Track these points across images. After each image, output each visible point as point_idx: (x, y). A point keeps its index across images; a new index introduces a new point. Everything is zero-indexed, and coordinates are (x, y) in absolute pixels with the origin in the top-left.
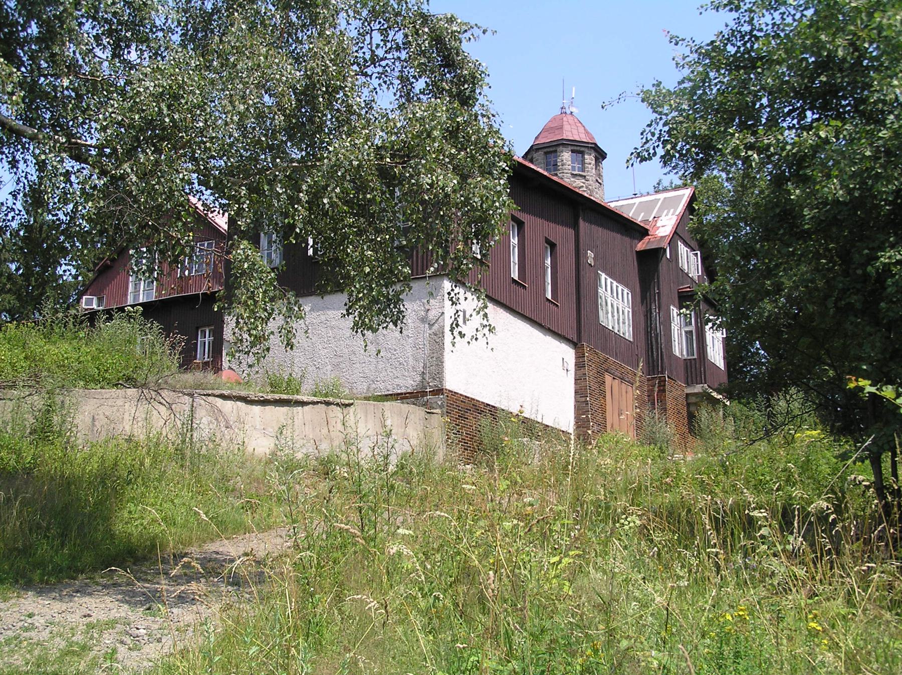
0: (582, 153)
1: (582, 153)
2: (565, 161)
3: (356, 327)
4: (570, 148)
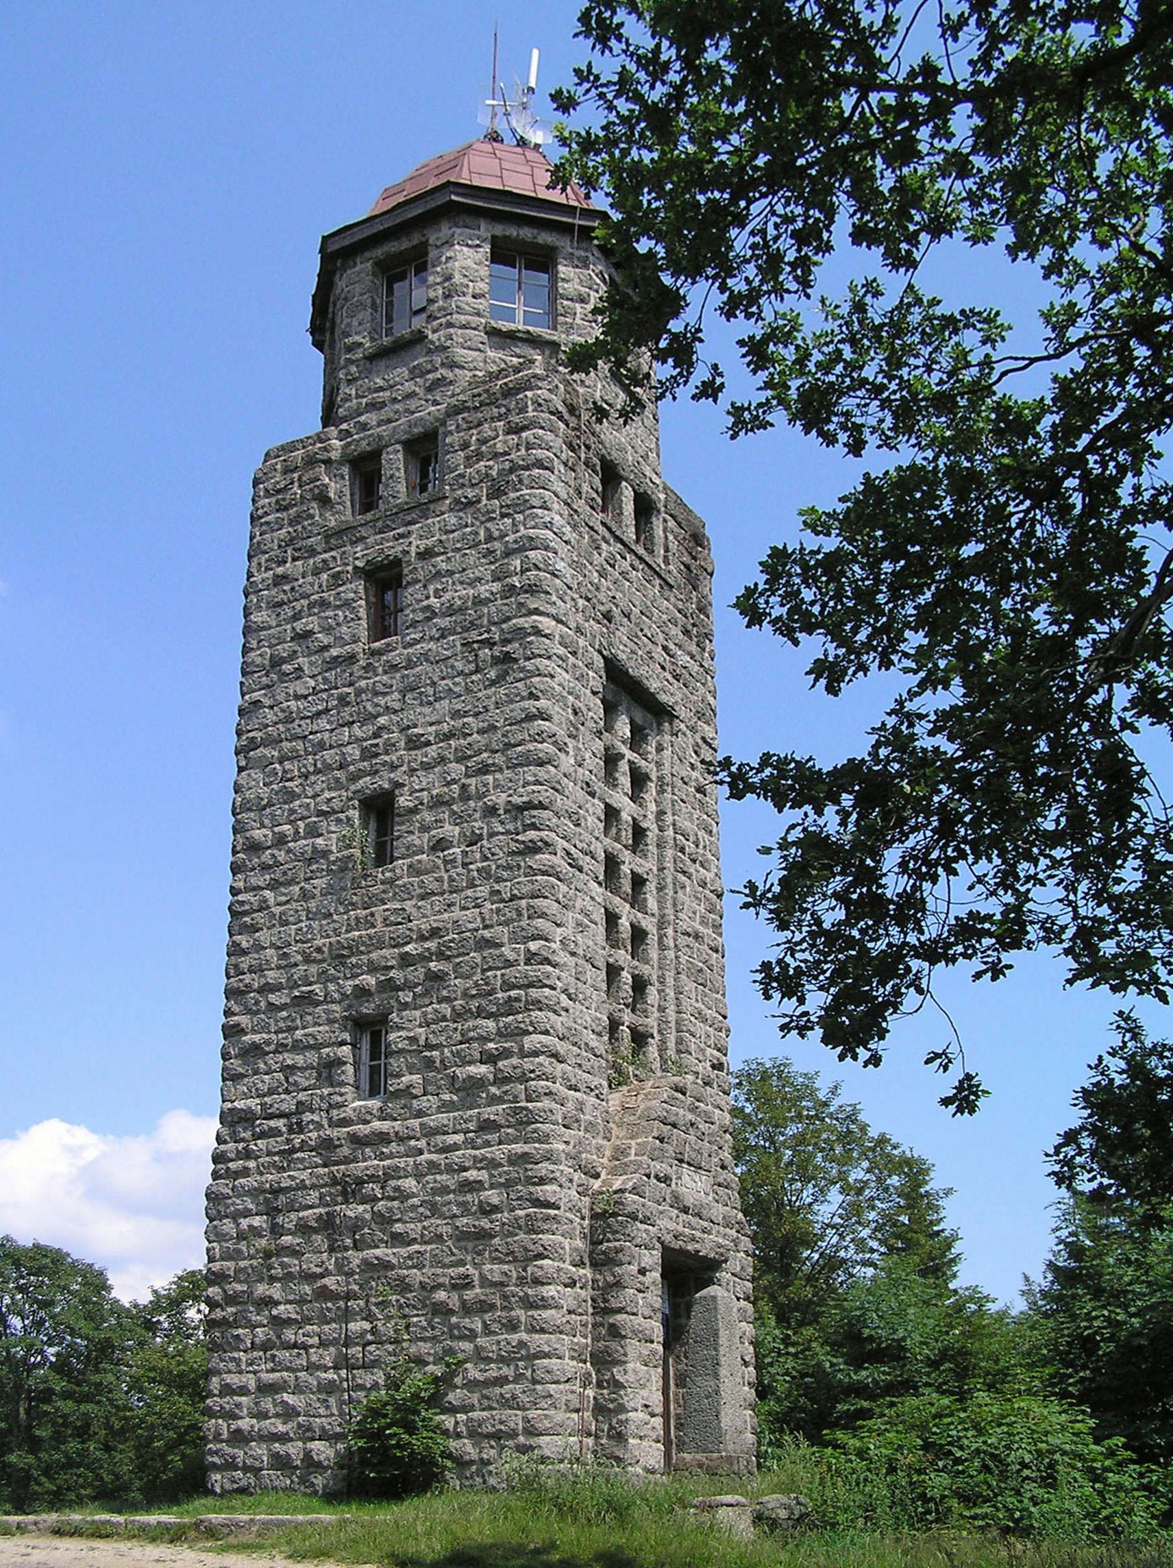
0: (543, 261)
1: (543, 261)
2: (457, 278)
3: (970, 1113)
4: (486, 229)
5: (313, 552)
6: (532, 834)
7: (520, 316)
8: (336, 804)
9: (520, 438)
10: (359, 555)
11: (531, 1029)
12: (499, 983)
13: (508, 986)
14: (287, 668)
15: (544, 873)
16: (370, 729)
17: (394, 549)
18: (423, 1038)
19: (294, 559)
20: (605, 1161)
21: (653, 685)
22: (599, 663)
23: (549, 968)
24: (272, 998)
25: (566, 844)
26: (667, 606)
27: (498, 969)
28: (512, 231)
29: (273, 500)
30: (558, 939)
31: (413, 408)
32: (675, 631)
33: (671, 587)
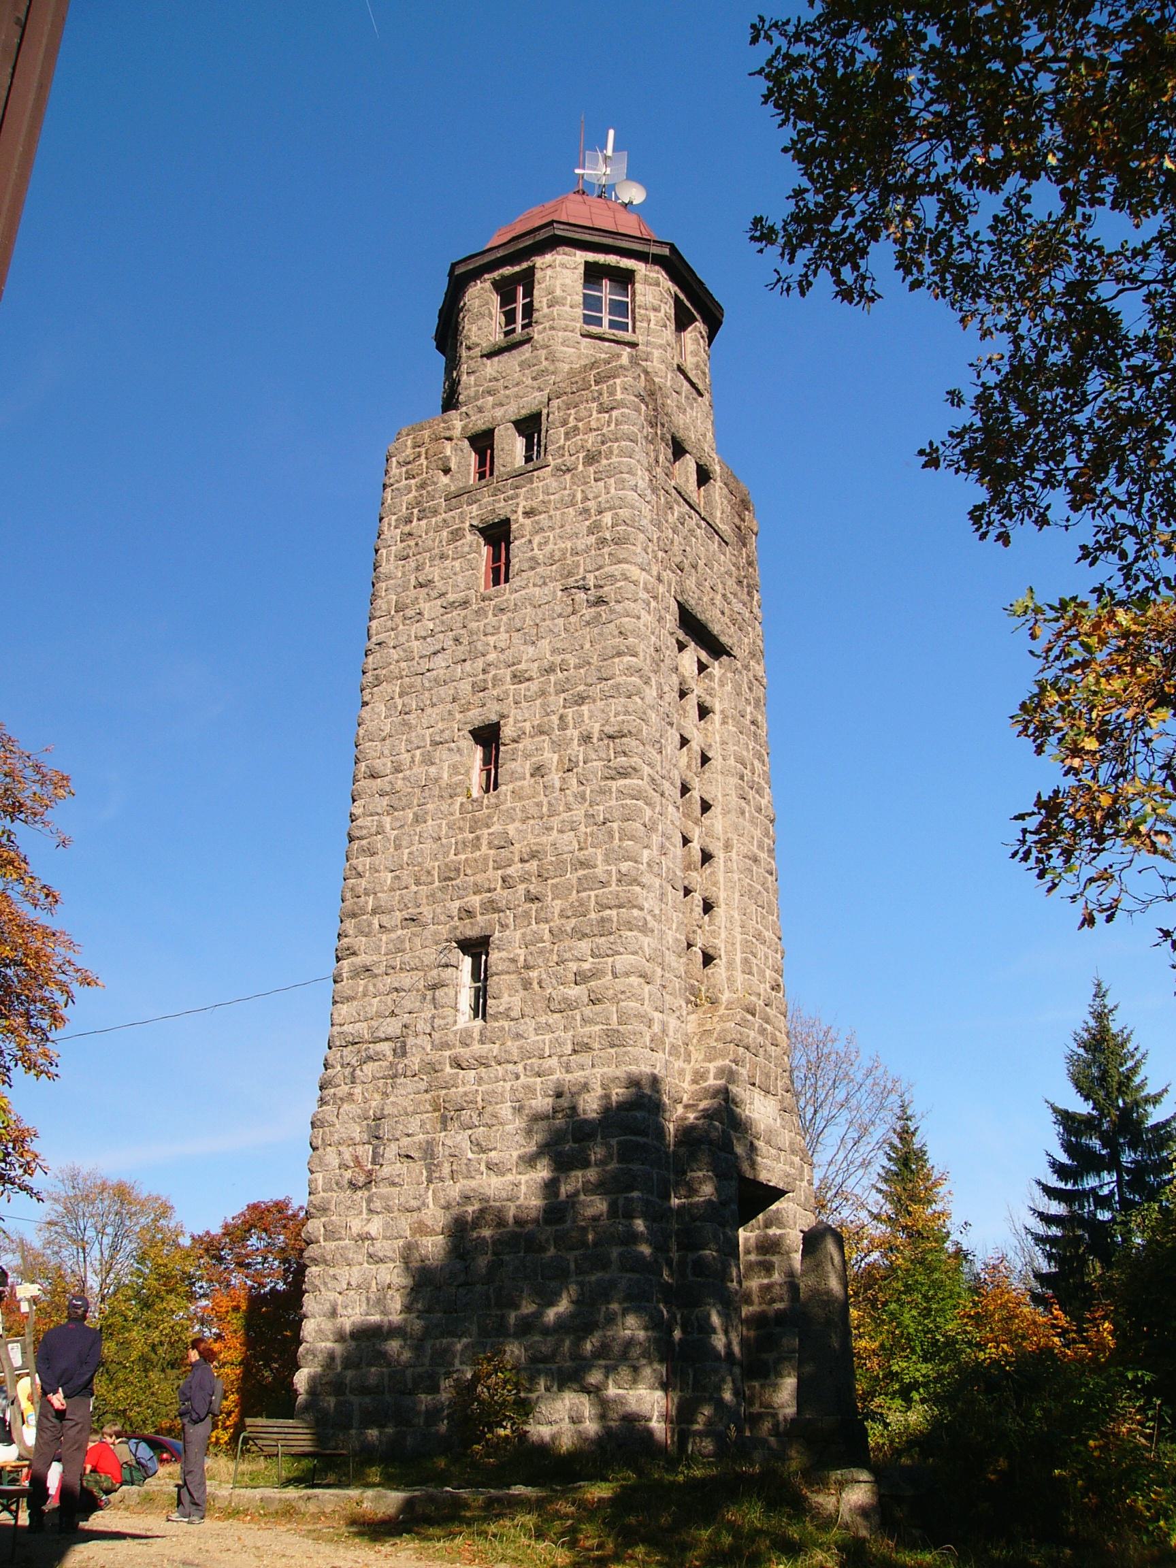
2: (558, 293)
4: (582, 257)
5: (435, 512)
6: (622, 760)
7: (606, 322)
8: (446, 735)
9: (610, 417)
10: (474, 513)
11: (622, 950)
12: (593, 903)
13: (603, 907)
14: (409, 613)
15: (634, 798)
16: (480, 663)
17: (503, 509)
18: (522, 958)
19: (419, 519)
20: (686, 1085)
21: (716, 629)
22: (674, 607)
23: (638, 889)
24: (385, 920)
25: (651, 771)
26: (726, 559)
27: (592, 889)
28: (601, 258)
29: (404, 469)
30: (645, 861)
31: (521, 394)
32: (731, 582)
33: (727, 543)
